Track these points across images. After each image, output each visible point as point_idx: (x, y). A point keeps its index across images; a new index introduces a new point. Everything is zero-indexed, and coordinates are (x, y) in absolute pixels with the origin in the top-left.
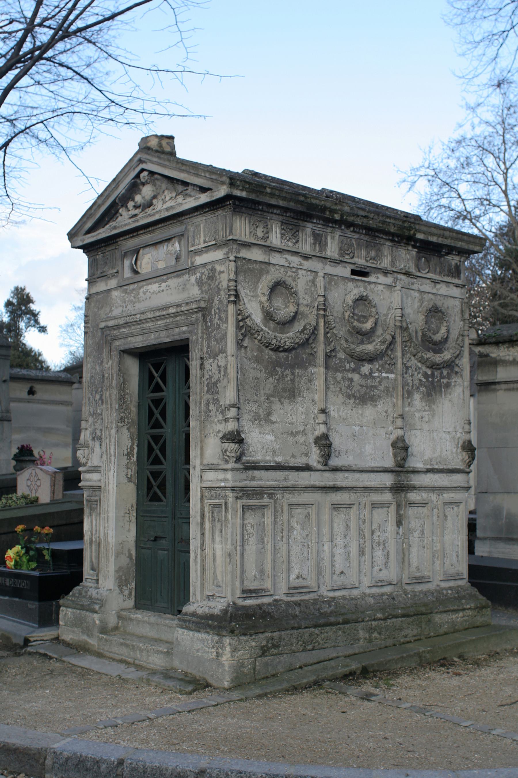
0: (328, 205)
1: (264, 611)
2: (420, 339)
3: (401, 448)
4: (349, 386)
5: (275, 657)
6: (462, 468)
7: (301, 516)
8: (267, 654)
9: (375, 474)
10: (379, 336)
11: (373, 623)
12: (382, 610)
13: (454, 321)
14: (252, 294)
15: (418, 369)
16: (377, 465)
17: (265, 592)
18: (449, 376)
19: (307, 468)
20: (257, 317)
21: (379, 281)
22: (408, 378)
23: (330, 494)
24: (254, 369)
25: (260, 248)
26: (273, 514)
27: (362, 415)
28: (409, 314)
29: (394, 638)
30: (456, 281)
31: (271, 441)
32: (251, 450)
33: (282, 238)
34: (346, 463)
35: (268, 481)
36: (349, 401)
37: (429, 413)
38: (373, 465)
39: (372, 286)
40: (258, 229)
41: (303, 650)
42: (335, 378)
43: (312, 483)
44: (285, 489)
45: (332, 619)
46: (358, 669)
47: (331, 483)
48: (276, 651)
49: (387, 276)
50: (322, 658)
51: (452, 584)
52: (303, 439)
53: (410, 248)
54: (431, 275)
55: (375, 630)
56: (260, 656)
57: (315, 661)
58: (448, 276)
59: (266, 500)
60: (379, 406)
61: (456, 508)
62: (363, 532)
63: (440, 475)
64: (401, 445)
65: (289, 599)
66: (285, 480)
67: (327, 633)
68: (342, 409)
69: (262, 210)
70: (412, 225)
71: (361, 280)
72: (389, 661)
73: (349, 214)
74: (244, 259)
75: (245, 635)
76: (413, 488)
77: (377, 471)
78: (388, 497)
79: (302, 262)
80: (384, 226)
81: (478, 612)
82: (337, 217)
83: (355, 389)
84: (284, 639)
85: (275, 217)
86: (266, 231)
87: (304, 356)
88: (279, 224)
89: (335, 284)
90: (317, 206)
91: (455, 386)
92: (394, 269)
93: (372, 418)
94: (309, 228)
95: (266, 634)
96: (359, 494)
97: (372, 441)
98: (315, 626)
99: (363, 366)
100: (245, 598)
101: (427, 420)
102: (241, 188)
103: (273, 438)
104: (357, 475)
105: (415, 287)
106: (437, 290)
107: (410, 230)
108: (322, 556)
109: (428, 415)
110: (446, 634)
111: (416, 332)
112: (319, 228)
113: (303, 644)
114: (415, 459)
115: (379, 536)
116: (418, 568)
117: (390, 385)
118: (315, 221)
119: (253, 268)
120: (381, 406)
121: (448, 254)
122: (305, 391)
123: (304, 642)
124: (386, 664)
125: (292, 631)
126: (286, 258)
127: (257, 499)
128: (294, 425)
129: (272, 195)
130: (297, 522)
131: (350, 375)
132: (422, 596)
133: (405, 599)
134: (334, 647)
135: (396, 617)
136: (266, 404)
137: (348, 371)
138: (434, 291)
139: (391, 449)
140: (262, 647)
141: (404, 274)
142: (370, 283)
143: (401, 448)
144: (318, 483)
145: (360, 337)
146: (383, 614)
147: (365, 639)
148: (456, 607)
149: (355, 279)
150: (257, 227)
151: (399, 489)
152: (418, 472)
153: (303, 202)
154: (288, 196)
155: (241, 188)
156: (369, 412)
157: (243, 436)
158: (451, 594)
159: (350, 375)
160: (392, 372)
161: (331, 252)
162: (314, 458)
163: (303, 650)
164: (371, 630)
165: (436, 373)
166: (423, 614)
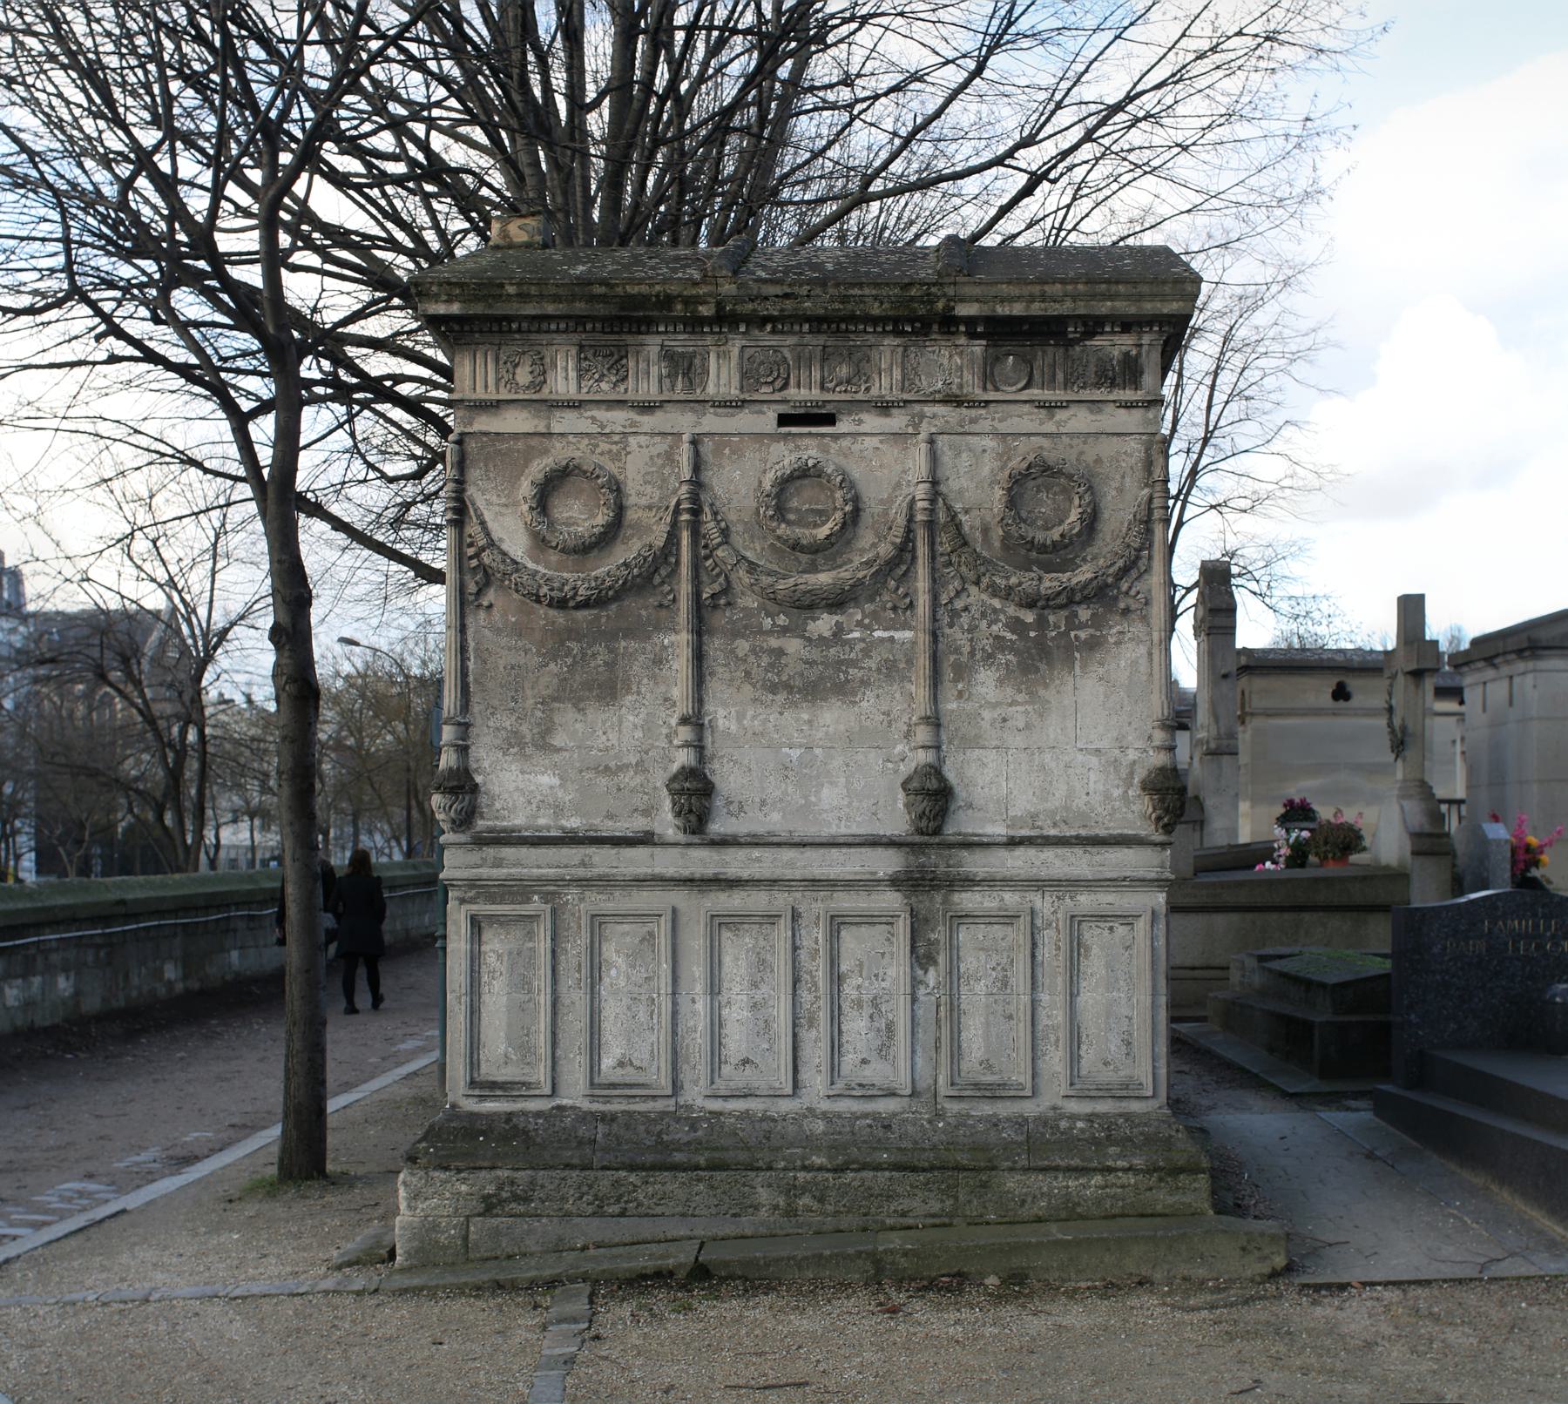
0: (673, 289)
1: (515, 1126)
2: (997, 544)
3: (934, 796)
4: (772, 665)
5: (519, 1220)
6: (1143, 833)
7: (628, 939)
8: (498, 1211)
9: (844, 850)
10: (863, 551)
11: (801, 1175)
12: (834, 1148)
13: (1120, 490)
14: (503, 500)
15: (990, 615)
16: (855, 830)
17: (528, 1089)
18: (1097, 622)
19: (646, 839)
20: (515, 542)
21: (863, 428)
22: (959, 635)
23: (712, 895)
24: (510, 649)
25: (524, 407)
26: (549, 933)
27: (810, 722)
28: (960, 492)
29: (865, 1215)
30: (1128, 395)
31: (551, 787)
32: (498, 805)
33: (580, 378)
34: (760, 829)
35: (539, 867)
36: (770, 697)
37: (1030, 708)
38: (843, 831)
39: (845, 443)
40: (518, 370)
41: (594, 1214)
42: (733, 651)
43: (657, 870)
44: (584, 883)
45: (678, 1157)
46: (680, 1265)
47: (710, 872)
48: (521, 1209)
49: (888, 415)
50: (647, 1235)
51: (1086, 1108)
52: (638, 779)
53: (962, 340)
54: (1036, 391)
55: (805, 1190)
56: (479, 1215)
57: (628, 1239)
58: (1098, 385)
59: (536, 905)
60: (864, 704)
61: (1121, 930)
62: (813, 977)
63: (1060, 851)
64: (933, 784)
65: (596, 1107)
66: (583, 864)
67: (664, 1184)
68: (750, 713)
69: (519, 331)
70: (934, 290)
71: (810, 434)
72: (778, 1260)
73: (737, 300)
74: (486, 434)
75: (447, 1169)
76: (969, 882)
77: (849, 845)
78: (891, 900)
79: (637, 418)
80: (849, 307)
81: (1161, 1180)
82: (705, 311)
83: (789, 671)
84: (542, 1186)
85: (558, 338)
86: (537, 369)
87: (644, 613)
88: (574, 351)
89: (733, 452)
90: (646, 297)
91: (1118, 643)
92: (906, 396)
93: (842, 727)
94: (653, 345)
95: (499, 1173)
96: (799, 895)
97: (843, 780)
98: (632, 1168)
99: (815, 619)
100: (482, 1098)
101: (1021, 725)
102: (444, 298)
103: (556, 781)
104: (788, 854)
105: (985, 425)
106: (1058, 424)
107: (931, 303)
108: (691, 1023)
109: (1026, 712)
110: (1039, 1220)
111: (986, 530)
112: (681, 342)
113: (647, 1206)
114: (979, 815)
115: (859, 987)
116: (987, 1065)
117: (900, 656)
118: (662, 329)
119: (509, 449)
120: (868, 702)
121: (1090, 334)
122: (645, 681)
123: (596, 1197)
124: (767, 1265)
125: (567, 1173)
126: (593, 418)
127: (512, 903)
128: (612, 753)
129: (523, 297)
130: (618, 952)
131: (774, 642)
132: (981, 1127)
133: (924, 1132)
134: (683, 1215)
135: (878, 1168)
136: (539, 714)
137: (770, 633)
138: (1050, 427)
139: (901, 795)
140: (486, 1198)
141: (944, 402)
142: (836, 437)
143: (934, 796)
144: (671, 871)
145: (804, 558)
146: (830, 1158)
147: (776, 1207)
148: (1076, 1162)
149: (789, 434)
150: (516, 366)
151: (912, 883)
152: (988, 845)
153: (605, 295)
154: (561, 291)
155: (444, 298)
156: (832, 717)
157: (479, 779)
158: (1082, 1131)
159: (774, 642)
160: (905, 626)
161: (718, 385)
162: (666, 823)
163: (594, 1214)
164: (792, 1190)
165: (1051, 618)
166: (959, 1168)
